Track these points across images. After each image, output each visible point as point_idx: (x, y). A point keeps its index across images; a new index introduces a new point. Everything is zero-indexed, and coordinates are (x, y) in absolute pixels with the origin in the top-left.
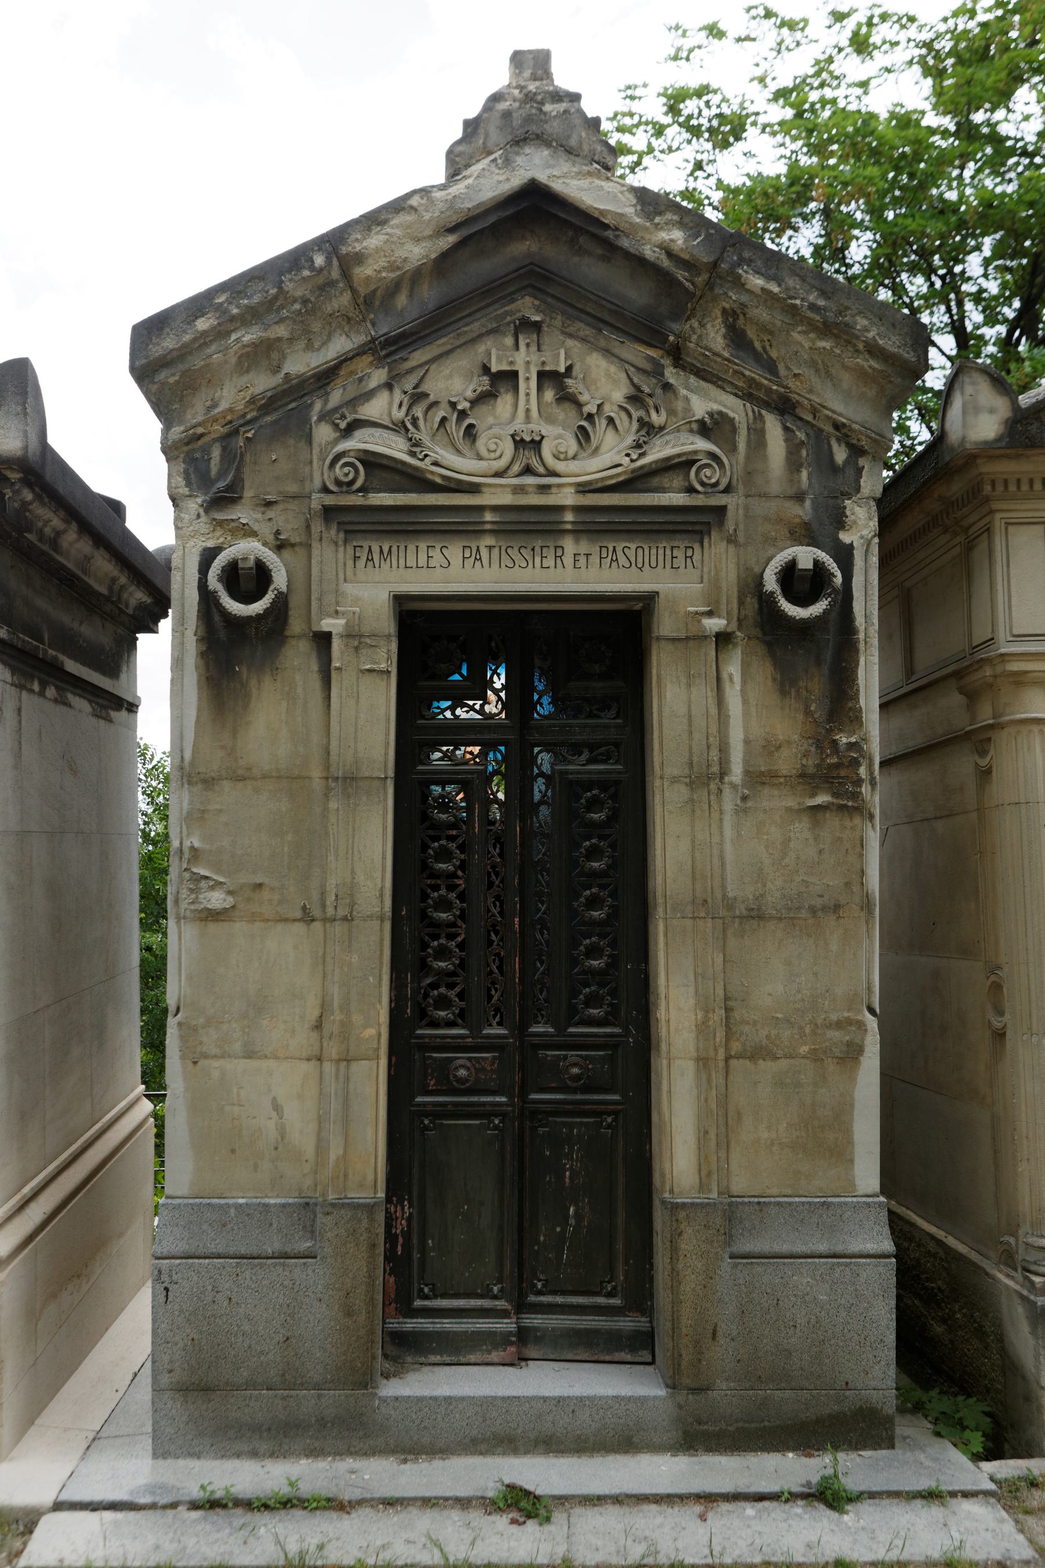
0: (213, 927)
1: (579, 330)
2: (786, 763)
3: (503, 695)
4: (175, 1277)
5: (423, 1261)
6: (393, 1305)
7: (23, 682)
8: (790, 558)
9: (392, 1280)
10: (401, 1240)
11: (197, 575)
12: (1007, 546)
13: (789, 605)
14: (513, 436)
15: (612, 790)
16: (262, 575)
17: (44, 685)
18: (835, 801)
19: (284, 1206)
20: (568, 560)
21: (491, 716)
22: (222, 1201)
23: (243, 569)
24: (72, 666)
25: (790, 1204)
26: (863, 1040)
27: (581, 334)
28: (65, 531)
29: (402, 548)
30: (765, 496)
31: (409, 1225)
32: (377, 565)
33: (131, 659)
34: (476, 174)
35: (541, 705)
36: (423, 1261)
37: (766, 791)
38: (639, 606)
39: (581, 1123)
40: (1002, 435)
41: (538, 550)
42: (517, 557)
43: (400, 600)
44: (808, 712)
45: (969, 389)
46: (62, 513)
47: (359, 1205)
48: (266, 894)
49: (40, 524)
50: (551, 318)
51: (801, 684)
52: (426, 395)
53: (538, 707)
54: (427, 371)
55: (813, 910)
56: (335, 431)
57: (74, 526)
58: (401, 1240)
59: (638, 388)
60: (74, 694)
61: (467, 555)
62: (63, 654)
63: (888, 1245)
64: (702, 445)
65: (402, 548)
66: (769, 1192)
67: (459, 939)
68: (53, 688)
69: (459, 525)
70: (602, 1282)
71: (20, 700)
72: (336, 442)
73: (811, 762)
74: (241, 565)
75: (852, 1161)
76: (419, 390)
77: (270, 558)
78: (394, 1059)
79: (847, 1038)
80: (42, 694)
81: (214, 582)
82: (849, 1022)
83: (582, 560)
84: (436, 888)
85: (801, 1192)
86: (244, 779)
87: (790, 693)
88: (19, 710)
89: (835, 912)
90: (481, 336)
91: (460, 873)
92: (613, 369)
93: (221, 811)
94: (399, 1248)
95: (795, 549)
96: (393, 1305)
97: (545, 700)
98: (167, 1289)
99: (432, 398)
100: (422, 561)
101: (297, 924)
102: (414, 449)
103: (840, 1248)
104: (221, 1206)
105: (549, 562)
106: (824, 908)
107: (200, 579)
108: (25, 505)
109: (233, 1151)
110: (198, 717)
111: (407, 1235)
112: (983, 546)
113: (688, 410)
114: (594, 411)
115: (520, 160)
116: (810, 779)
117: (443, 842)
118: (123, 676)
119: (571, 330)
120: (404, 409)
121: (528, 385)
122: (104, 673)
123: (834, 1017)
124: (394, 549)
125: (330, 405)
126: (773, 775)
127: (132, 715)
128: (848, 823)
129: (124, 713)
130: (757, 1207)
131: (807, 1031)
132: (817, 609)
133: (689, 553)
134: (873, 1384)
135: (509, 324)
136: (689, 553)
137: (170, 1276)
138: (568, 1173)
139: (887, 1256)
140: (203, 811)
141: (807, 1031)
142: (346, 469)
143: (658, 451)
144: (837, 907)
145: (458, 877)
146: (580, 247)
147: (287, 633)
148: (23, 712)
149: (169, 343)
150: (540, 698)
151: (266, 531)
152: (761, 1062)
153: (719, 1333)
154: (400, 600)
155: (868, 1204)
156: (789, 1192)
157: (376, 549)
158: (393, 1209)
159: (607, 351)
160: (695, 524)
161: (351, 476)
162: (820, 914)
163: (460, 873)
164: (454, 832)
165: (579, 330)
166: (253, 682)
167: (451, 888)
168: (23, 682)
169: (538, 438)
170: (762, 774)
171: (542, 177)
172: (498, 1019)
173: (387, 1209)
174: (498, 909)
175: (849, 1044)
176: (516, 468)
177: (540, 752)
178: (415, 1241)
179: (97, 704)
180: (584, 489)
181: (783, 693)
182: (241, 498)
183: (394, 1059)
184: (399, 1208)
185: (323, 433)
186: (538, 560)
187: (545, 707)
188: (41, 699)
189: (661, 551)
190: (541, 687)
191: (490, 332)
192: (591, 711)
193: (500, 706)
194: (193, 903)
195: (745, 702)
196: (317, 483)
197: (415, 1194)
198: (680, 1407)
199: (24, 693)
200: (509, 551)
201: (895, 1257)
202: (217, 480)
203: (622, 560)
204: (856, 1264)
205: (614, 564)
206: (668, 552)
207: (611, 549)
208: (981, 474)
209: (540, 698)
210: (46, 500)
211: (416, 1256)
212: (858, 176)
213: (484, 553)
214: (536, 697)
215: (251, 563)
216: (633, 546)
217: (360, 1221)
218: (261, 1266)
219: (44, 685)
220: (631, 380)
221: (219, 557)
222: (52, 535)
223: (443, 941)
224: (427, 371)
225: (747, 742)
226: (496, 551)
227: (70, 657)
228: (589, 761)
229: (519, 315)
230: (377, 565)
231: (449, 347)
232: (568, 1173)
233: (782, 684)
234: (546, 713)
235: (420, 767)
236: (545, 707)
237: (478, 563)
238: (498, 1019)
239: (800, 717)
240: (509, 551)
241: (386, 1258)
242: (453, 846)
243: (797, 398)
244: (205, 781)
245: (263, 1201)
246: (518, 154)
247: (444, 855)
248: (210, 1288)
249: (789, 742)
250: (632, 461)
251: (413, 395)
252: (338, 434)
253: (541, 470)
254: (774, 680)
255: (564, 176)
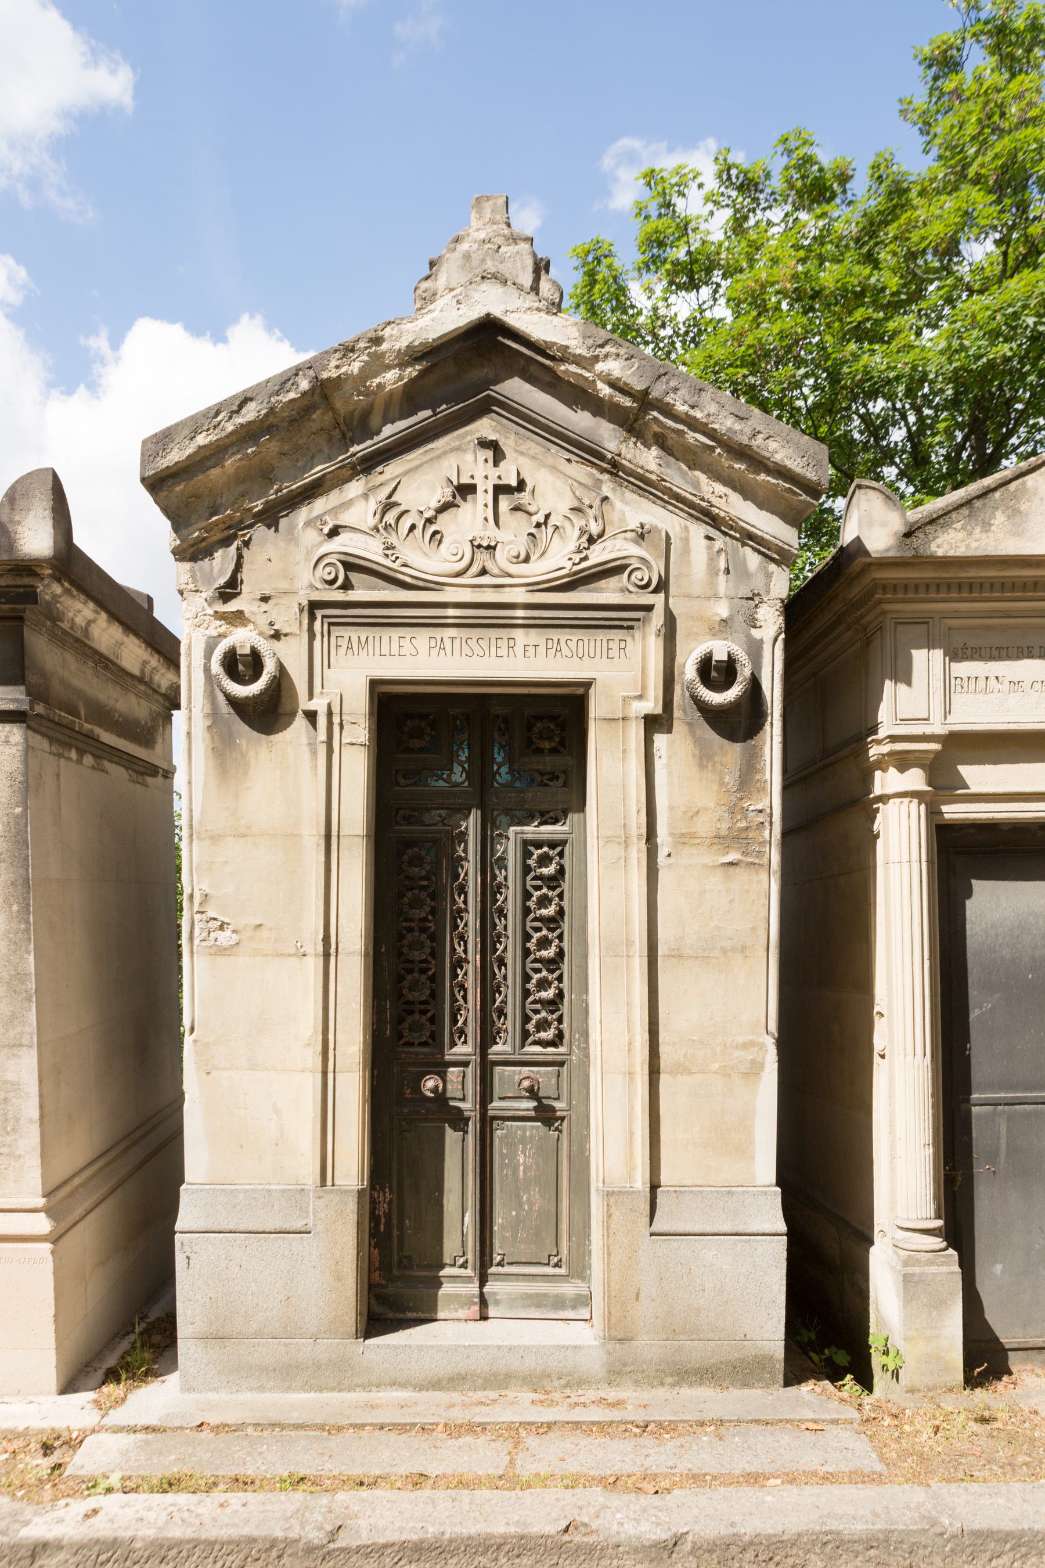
0: (221, 961)
1: (529, 449)
2: (705, 826)
3: (466, 766)
4: (195, 1248)
5: (401, 1238)
6: (378, 1272)
7: (61, 751)
8: (708, 650)
9: (376, 1251)
10: (383, 1220)
11: (203, 661)
12: (895, 642)
13: (265, 672)
14: (471, 541)
15: (559, 849)
16: (255, 661)
17: (81, 753)
18: (744, 859)
19: (283, 1191)
20: (519, 649)
21: (458, 785)
22: (232, 1187)
23: (240, 655)
24: (108, 738)
25: (701, 1192)
26: (764, 1059)
27: (532, 452)
28: (94, 621)
29: (377, 639)
30: (689, 596)
31: (390, 1208)
32: (356, 653)
33: (167, 732)
34: (439, 308)
35: (500, 775)
36: (401, 1238)
37: (686, 850)
38: (581, 691)
39: (533, 1127)
40: (891, 546)
41: (493, 641)
42: (476, 647)
43: (374, 684)
44: (722, 784)
45: (864, 505)
46: (91, 605)
47: (346, 1191)
48: (264, 933)
49: (71, 615)
50: (506, 438)
51: (716, 759)
52: (396, 504)
53: (498, 777)
54: (399, 483)
55: (724, 951)
56: (320, 535)
57: (104, 616)
58: (383, 1220)
59: (580, 500)
60: (110, 761)
61: (433, 644)
62: (100, 726)
63: (783, 1227)
64: (634, 550)
65: (377, 639)
66: (684, 1183)
67: (430, 973)
68: (90, 756)
69: (426, 617)
70: (549, 1256)
71: (58, 766)
72: (320, 544)
73: (725, 825)
74: (239, 652)
75: (753, 1158)
76: (393, 499)
77: (265, 647)
78: (376, 1072)
79: (751, 1057)
80: (79, 761)
81: (216, 668)
82: (753, 1044)
83: (531, 651)
84: (410, 930)
85: (711, 1183)
86: (244, 836)
87: (707, 767)
88: (58, 775)
89: (742, 952)
90: (445, 453)
91: (430, 917)
92: (559, 483)
93: (226, 863)
94: (382, 1227)
95: (711, 643)
96: (378, 1272)
97: (504, 770)
98: (188, 1258)
99: (402, 508)
100: (395, 649)
101: (291, 959)
102: (387, 552)
103: (741, 1229)
104: (232, 1191)
105: (503, 652)
106: (733, 949)
107: (205, 664)
108: (55, 597)
109: (241, 1146)
110: (205, 782)
111: (388, 1216)
112: (876, 643)
113: (623, 520)
114: (542, 521)
115: (477, 296)
116: (723, 841)
117: (416, 891)
118: (159, 747)
119: (522, 448)
120: (378, 516)
121: (484, 497)
122: (140, 744)
123: (740, 1040)
124: (370, 639)
125: (315, 514)
126: (693, 836)
127: (168, 781)
128: (755, 878)
129: (160, 779)
130: (673, 1195)
131: (718, 1050)
132: (733, 693)
133: (512, 644)
134: (766, 1336)
135: (469, 442)
136: (623, 645)
137: (191, 1247)
138: (522, 1168)
139: (781, 1235)
140: (211, 863)
141: (718, 1050)
142: (328, 569)
143: (598, 555)
144: (744, 948)
145: (430, 922)
146: (531, 375)
147: (280, 711)
148: (62, 778)
149: (176, 456)
150: (499, 768)
151: (262, 621)
152: (679, 1076)
153: (642, 1295)
154: (374, 684)
155: (766, 1193)
156: (701, 1183)
157: (355, 640)
158: (376, 1195)
159: (554, 468)
160: (622, 619)
161: (332, 576)
162: (730, 954)
163: (430, 917)
164: (426, 883)
165: (529, 449)
166: (251, 753)
167: (423, 930)
168: (61, 751)
169: (493, 544)
170: (683, 835)
171: (497, 312)
172: (462, 1039)
173: (371, 1195)
174: (462, 947)
175: (753, 1062)
176: (475, 569)
177: (499, 815)
178: (395, 1221)
179: (134, 771)
180: (535, 587)
181: (702, 766)
182: (239, 593)
183: (376, 1072)
184: (381, 1194)
185: (310, 537)
186: (493, 649)
187: (504, 775)
188: (79, 766)
189: (598, 644)
190: (499, 759)
191: (452, 450)
192: (542, 781)
193: (464, 775)
194: (204, 940)
195: (670, 774)
196: (306, 583)
197: (395, 1183)
198: (610, 1354)
199: (62, 760)
200: (469, 641)
201: (786, 1235)
202: (219, 577)
203: (565, 651)
204: (754, 1240)
205: (559, 654)
206: (605, 644)
207: (556, 641)
208: (874, 579)
209: (499, 768)
210: (75, 593)
211: (395, 1233)
212: (868, 319)
213: (447, 643)
214: (495, 768)
215: (247, 651)
216: (575, 639)
217: (346, 1204)
218: (283, 1238)
219: (81, 753)
220: (574, 493)
221: (220, 645)
222: (84, 625)
223: (416, 975)
224: (399, 483)
225: (671, 808)
226: (457, 642)
227: (106, 730)
228: (540, 824)
229: (478, 435)
230: (356, 653)
231: (417, 463)
232: (522, 1168)
233: (701, 758)
234: (504, 782)
235: (397, 827)
236: (504, 775)
237: (442, 652)
238: (462, 1039)
239: (715, 787)
240: (469, 641)
241: (371, 1235)
242: (424, 895)
243: (717, 511)
244: (212, 837)
245: (267, 1187)
246: (476, 291)
247: (416, 903)
248: (224, 1257)
249: (706, 809)
250: (574, 564)
251: (387, 505)
252: (322, 538)
253: (496, 571)
254: (694, 756)
255: (517, 311)
